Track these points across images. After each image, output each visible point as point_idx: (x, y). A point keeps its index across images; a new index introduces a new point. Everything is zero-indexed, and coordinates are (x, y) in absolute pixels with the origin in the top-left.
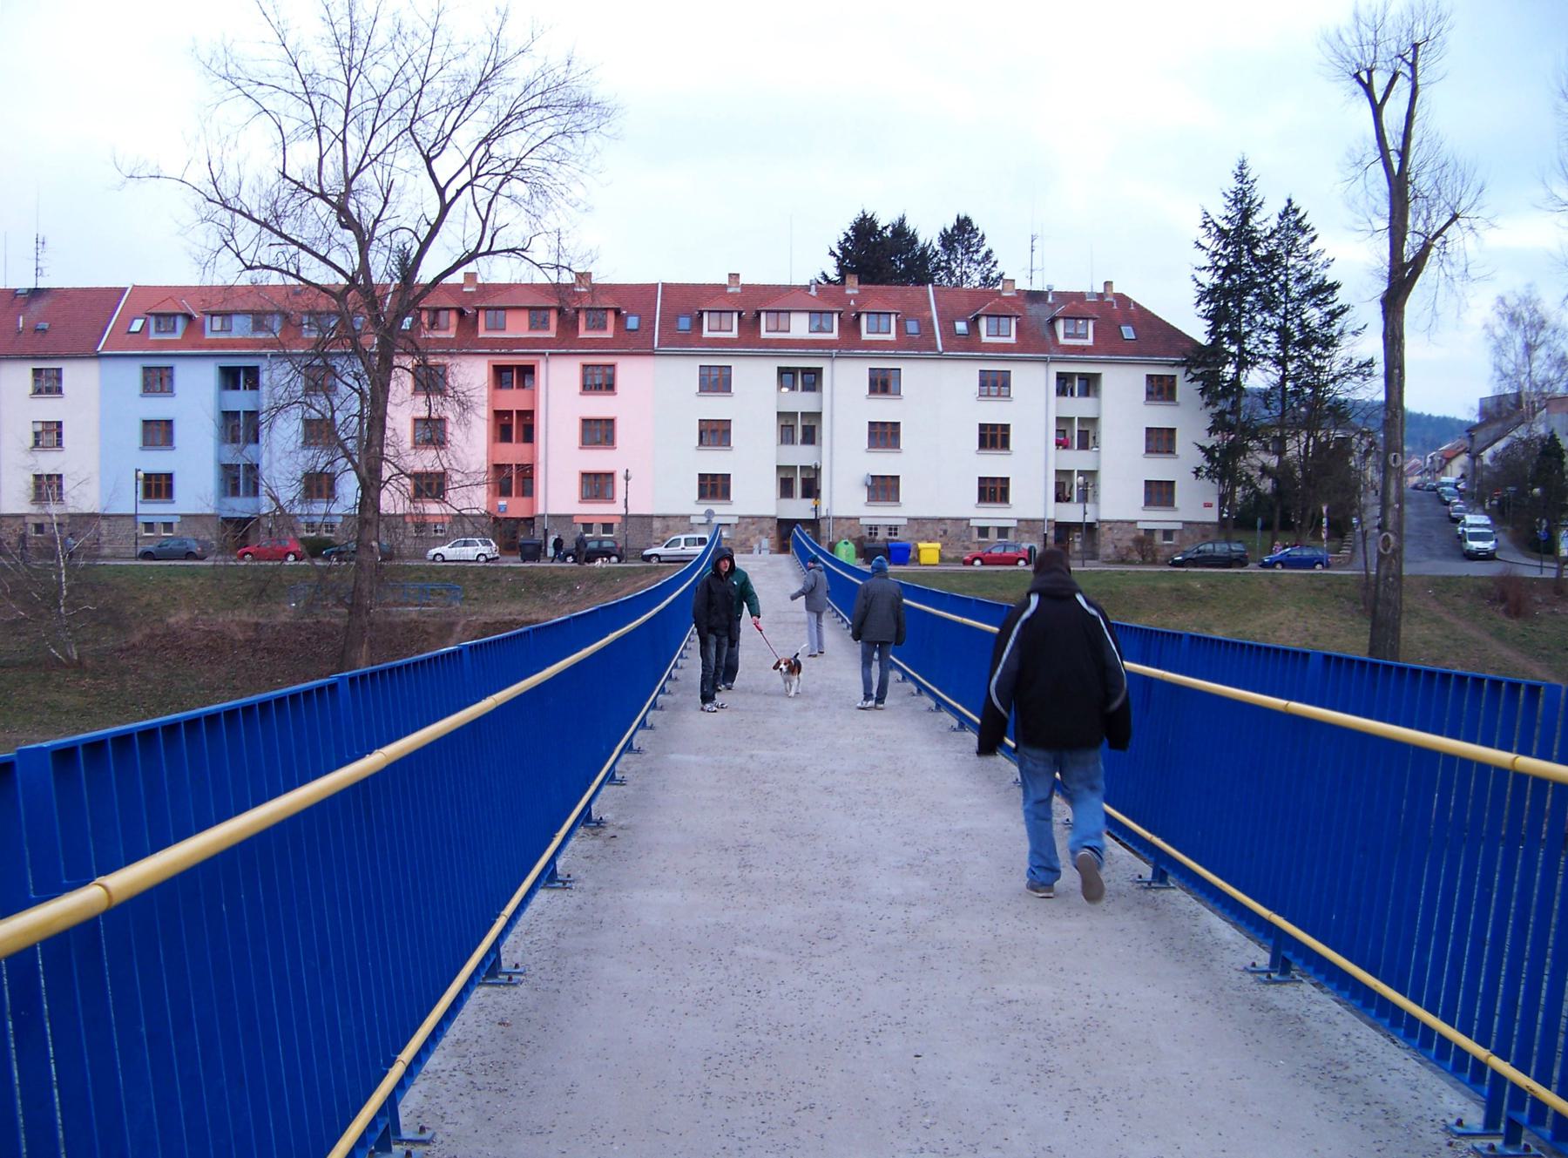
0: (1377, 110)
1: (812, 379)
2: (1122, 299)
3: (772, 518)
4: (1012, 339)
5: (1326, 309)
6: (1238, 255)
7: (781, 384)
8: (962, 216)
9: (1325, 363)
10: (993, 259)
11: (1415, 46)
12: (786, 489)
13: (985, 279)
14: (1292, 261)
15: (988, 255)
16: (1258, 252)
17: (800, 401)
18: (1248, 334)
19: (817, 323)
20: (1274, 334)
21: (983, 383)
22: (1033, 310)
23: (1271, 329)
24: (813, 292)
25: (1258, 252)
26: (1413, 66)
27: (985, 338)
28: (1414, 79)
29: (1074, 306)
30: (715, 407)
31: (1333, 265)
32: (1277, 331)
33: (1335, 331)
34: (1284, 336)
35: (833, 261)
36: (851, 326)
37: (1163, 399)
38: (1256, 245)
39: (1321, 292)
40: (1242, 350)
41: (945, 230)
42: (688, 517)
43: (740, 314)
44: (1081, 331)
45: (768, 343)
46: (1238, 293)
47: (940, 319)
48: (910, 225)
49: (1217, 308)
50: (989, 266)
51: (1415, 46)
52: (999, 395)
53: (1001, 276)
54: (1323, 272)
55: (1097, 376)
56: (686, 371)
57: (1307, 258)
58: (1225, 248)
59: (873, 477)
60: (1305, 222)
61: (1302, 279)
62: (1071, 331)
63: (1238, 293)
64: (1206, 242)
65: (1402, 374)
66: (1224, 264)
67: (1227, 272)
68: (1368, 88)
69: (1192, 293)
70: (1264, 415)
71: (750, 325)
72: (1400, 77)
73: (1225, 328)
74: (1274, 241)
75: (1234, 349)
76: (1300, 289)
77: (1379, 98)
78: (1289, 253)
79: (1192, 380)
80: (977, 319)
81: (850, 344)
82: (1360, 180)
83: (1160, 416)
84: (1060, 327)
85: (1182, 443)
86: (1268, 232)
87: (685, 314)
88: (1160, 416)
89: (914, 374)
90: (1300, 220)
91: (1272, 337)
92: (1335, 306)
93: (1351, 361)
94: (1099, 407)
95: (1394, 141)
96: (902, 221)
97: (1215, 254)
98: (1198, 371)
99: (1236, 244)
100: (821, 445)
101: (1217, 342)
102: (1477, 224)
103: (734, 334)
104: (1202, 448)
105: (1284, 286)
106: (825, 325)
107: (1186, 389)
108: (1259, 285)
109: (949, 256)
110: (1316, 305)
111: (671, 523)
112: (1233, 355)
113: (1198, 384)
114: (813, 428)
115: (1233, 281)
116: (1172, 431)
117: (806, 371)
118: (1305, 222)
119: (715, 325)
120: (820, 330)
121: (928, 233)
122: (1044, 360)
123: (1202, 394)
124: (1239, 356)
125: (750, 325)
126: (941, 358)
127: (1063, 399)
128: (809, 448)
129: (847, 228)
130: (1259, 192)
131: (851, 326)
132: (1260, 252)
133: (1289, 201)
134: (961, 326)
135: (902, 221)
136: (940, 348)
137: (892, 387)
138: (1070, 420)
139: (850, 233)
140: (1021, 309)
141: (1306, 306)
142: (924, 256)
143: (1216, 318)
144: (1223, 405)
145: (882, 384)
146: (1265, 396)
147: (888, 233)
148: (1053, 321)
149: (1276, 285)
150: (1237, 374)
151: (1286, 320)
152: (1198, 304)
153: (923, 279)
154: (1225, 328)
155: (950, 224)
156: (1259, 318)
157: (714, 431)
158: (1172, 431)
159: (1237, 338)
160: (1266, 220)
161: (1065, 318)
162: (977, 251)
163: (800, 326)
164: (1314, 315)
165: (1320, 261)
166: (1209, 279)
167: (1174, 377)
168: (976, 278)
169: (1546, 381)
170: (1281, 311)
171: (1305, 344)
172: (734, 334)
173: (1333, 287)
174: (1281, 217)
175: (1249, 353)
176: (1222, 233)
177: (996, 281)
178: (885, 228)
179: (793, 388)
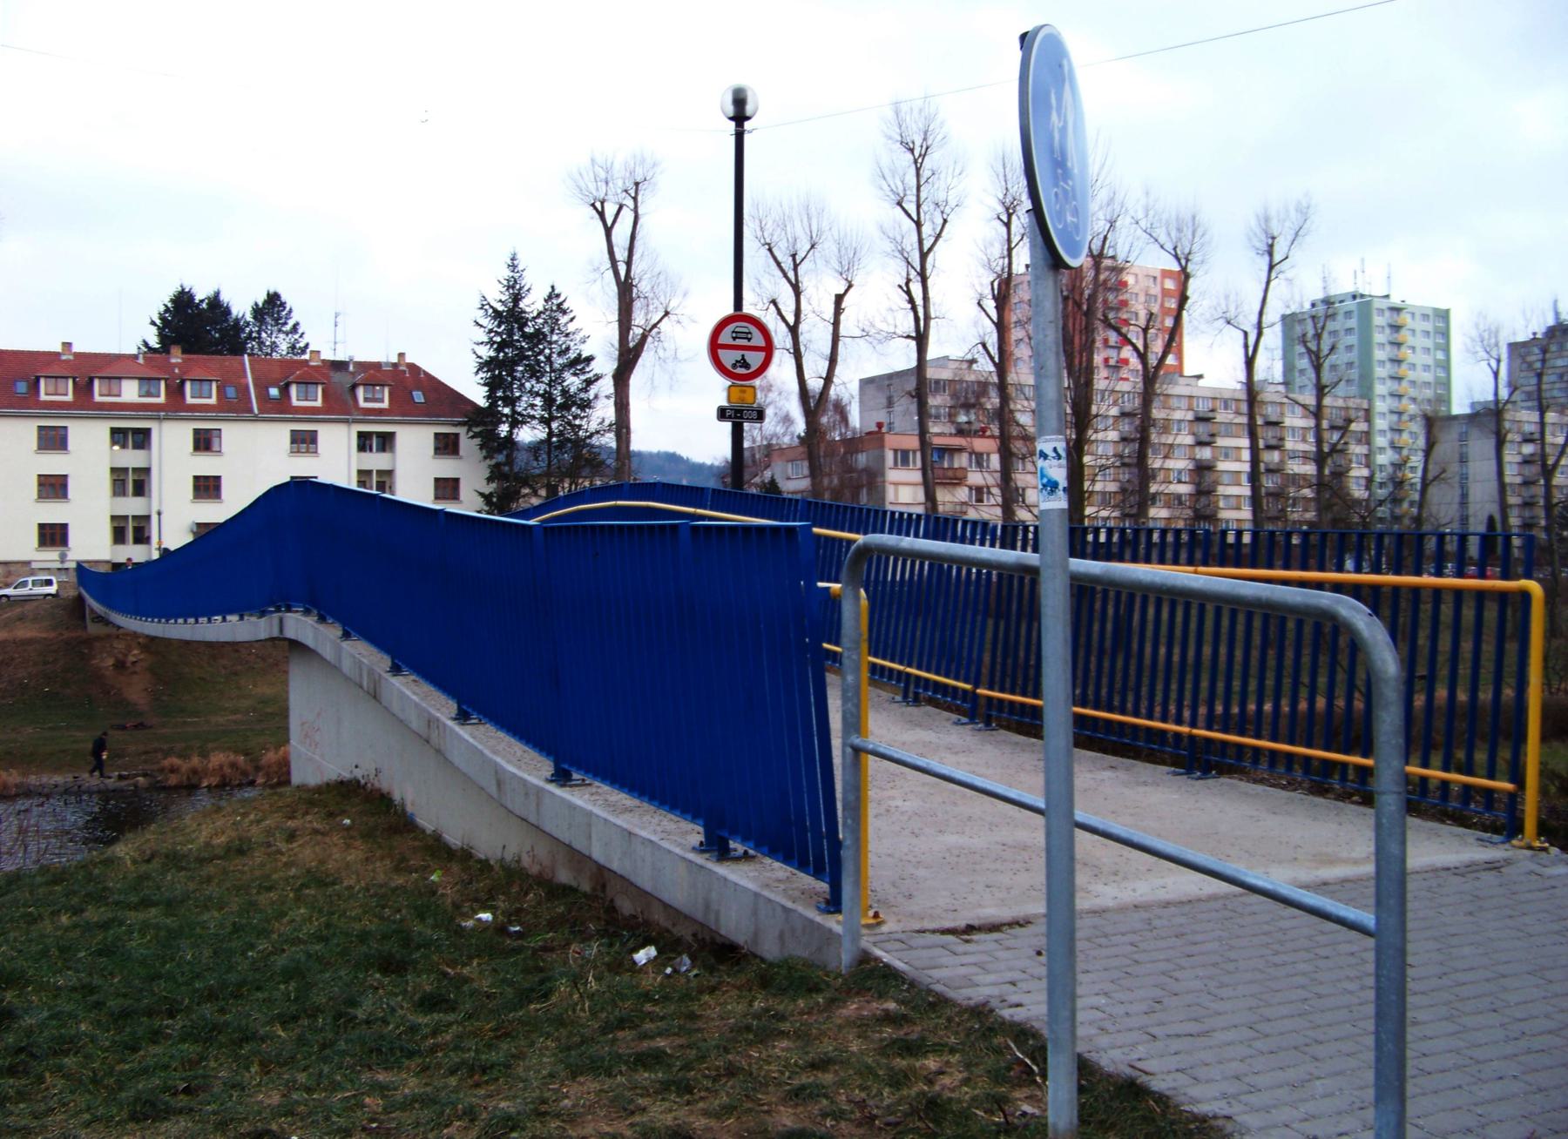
0: (608, 231)
1: (142, 439)
2: (414, 368)
3: (107, 562)
4: (319, 403)
5: (583, 377)
6: (510, 333)
7: (114, 442)
8: (272, 291)
9: (584, 422)
10: (300, 331)
11: (637, 184)
12: (119, 536)
13: (293, 347)
14: (555, 338)
15: (295, 328)
16: (527, 330)
17: (131, 458)
18: (519, 398)
19: (145, 389)
20: (539, 399)
21: (293, 441)
22: (337, 377)
23: (537, 394)
24: (141, 361)
25: (527, 330)
26: (635, 199)
27: (295, 402)
28: (636, 210)
29: (372, 374)
30: (53, 464)
31: (588, 341)
32: (542, 396)
33: (591, 394)
34: (549, 400)
35: (154, 330)
36: (176, 392)
37: (448, 454)
38: (525, 324)
39: (580, 363)
40: (514, 412)
41: (256, 304)
42: (28, 563)
43: (74, 379)
44: (378, 396)
45: (102, 406)
46: (509, 365)
47: (256, 385)
48: (225, 298)
49: (493, 377)
50: (296, 336)
51: (637, 184)
52: (307, 452)
53: (307, 346)
54: (582, 347)
55: (391, 435)
56: (279, 434)
57: (567, 335)
58: (499, 326)
59: (199, 525)
60: (565, 306)
61: (562, 353)
62: (370, 396)
63: (509, 365)
64: (485, 322)
65: (628, 432)
66: (498, 339)
67: (501, 347)
68: (602, 215)
69: (473, 364)
70: (539, 467)
71: (84, 389)
72: (625, 208)
73: (500, 394)
74: (540, 321)
75: (507, 411)
76: (561, 361)
77: (609, 223)
78: (552, 331)
79: (472, 437)
80: (287, 385)
81: (176, 407)
82: (599, 282)
83: (447, 468)
84: (360, 392)
85: (466, 491)
86: (535, 314)
87: (22, 379)
88: (447, 468)
89: (233, 434)
90: (561, 304)
91: (538, 401)
92: (591, 375)
93: (603, 421)
94: (394, 460)
95: (621, 255)
96: (217, 294)
97: (491, 331)
98: (477, 430)
99: (507, 322)
100: (150, 496)
101: (493, 405)
102: (682, 318)
103: (70, 398)
104: (482, 495)
105: (549, 358)
106: (153, 391)
107: (468, 445)
108: (527, 358)
109: (260, 327)
110: (575, 374)
111: (12, 568)
112: (506, 415)
113: (478, 441)
114: (143, 481)
115: (506, 354)
116: (457, 481)
117: (136, 431)
118: (565, 306)
119: (51, 389)
120: (149, 394)
121: (241, 306)
122: (346, 421)
123: (481, 449)
124: (512, 416)
125: (84, 389)
126: (256, 419)
127: (363, 454)
128: (139, 500)
129: (167, 301)
130: (527, 281)
131: (176, 392)
132: (529, 330)
133: (553, 287)
134: (274, 392)
135: (217, 294)
136: (256, 411)
137: (216, 448)
138: (369, 472)
139: (170, 305)
140: (328, 377)
141: (566, 375)
142: (237, 326)
143: (493, 385)
144: (501, 458)
145: (204, 442)
146: (535, 448)
147: (204, 305)
148: (354, 387)
149: (541, 358)
150: (510, 432)
151: (550, 386)
152: (477, 373)
153: (238, 348)
154: (500, 394)
155: (261, 298)
156: (528, 385)
157: (52, 485)
158: (457, 481)
159: (511, 401)
160: (533, 303)
161: (364, 385)
162: (285, 323)
163: (130, 392)
164: (573, 382)
165: (578, 337)
166: (486, 352)
167: (457, 435)
168: (284, 347)
169: (775, 435)
170: (546, 379)
171: (565, 407)
172: (70, 398)
173: (589, 359)
174: (546, 301)
175: (519, 414)
176: (497, 314)
177: (304, 350)
178: (202, 301)
179: (124, 446)
